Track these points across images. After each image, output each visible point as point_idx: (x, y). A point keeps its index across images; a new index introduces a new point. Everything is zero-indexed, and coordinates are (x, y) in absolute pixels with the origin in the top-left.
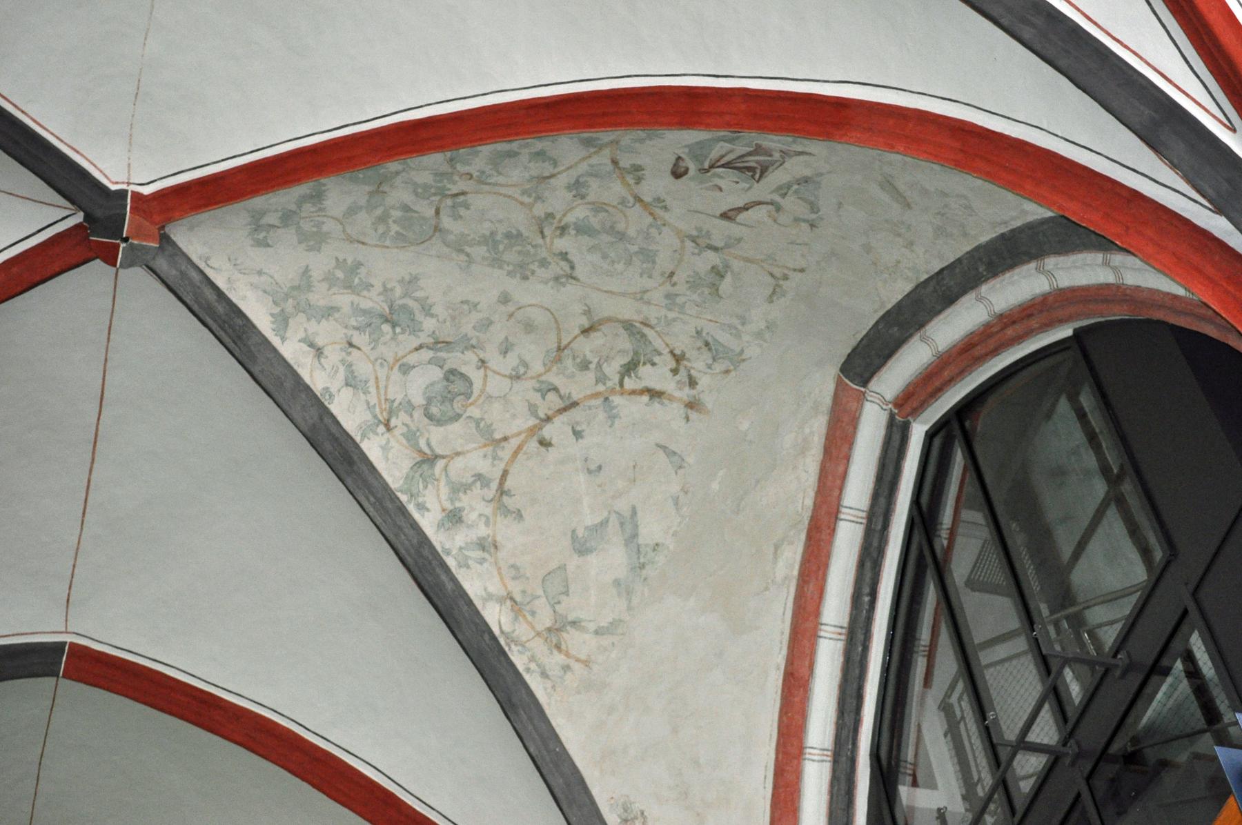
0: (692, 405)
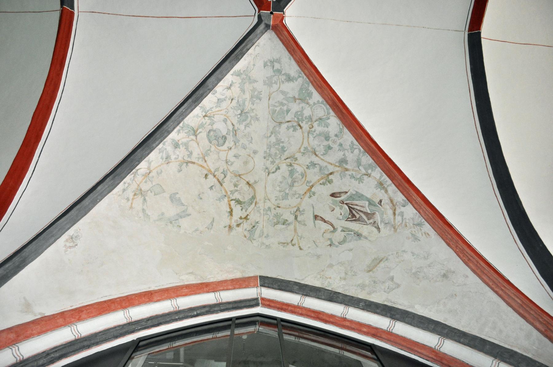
0: (230, 227)
